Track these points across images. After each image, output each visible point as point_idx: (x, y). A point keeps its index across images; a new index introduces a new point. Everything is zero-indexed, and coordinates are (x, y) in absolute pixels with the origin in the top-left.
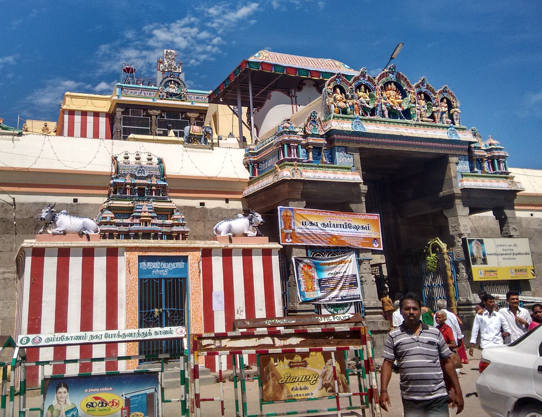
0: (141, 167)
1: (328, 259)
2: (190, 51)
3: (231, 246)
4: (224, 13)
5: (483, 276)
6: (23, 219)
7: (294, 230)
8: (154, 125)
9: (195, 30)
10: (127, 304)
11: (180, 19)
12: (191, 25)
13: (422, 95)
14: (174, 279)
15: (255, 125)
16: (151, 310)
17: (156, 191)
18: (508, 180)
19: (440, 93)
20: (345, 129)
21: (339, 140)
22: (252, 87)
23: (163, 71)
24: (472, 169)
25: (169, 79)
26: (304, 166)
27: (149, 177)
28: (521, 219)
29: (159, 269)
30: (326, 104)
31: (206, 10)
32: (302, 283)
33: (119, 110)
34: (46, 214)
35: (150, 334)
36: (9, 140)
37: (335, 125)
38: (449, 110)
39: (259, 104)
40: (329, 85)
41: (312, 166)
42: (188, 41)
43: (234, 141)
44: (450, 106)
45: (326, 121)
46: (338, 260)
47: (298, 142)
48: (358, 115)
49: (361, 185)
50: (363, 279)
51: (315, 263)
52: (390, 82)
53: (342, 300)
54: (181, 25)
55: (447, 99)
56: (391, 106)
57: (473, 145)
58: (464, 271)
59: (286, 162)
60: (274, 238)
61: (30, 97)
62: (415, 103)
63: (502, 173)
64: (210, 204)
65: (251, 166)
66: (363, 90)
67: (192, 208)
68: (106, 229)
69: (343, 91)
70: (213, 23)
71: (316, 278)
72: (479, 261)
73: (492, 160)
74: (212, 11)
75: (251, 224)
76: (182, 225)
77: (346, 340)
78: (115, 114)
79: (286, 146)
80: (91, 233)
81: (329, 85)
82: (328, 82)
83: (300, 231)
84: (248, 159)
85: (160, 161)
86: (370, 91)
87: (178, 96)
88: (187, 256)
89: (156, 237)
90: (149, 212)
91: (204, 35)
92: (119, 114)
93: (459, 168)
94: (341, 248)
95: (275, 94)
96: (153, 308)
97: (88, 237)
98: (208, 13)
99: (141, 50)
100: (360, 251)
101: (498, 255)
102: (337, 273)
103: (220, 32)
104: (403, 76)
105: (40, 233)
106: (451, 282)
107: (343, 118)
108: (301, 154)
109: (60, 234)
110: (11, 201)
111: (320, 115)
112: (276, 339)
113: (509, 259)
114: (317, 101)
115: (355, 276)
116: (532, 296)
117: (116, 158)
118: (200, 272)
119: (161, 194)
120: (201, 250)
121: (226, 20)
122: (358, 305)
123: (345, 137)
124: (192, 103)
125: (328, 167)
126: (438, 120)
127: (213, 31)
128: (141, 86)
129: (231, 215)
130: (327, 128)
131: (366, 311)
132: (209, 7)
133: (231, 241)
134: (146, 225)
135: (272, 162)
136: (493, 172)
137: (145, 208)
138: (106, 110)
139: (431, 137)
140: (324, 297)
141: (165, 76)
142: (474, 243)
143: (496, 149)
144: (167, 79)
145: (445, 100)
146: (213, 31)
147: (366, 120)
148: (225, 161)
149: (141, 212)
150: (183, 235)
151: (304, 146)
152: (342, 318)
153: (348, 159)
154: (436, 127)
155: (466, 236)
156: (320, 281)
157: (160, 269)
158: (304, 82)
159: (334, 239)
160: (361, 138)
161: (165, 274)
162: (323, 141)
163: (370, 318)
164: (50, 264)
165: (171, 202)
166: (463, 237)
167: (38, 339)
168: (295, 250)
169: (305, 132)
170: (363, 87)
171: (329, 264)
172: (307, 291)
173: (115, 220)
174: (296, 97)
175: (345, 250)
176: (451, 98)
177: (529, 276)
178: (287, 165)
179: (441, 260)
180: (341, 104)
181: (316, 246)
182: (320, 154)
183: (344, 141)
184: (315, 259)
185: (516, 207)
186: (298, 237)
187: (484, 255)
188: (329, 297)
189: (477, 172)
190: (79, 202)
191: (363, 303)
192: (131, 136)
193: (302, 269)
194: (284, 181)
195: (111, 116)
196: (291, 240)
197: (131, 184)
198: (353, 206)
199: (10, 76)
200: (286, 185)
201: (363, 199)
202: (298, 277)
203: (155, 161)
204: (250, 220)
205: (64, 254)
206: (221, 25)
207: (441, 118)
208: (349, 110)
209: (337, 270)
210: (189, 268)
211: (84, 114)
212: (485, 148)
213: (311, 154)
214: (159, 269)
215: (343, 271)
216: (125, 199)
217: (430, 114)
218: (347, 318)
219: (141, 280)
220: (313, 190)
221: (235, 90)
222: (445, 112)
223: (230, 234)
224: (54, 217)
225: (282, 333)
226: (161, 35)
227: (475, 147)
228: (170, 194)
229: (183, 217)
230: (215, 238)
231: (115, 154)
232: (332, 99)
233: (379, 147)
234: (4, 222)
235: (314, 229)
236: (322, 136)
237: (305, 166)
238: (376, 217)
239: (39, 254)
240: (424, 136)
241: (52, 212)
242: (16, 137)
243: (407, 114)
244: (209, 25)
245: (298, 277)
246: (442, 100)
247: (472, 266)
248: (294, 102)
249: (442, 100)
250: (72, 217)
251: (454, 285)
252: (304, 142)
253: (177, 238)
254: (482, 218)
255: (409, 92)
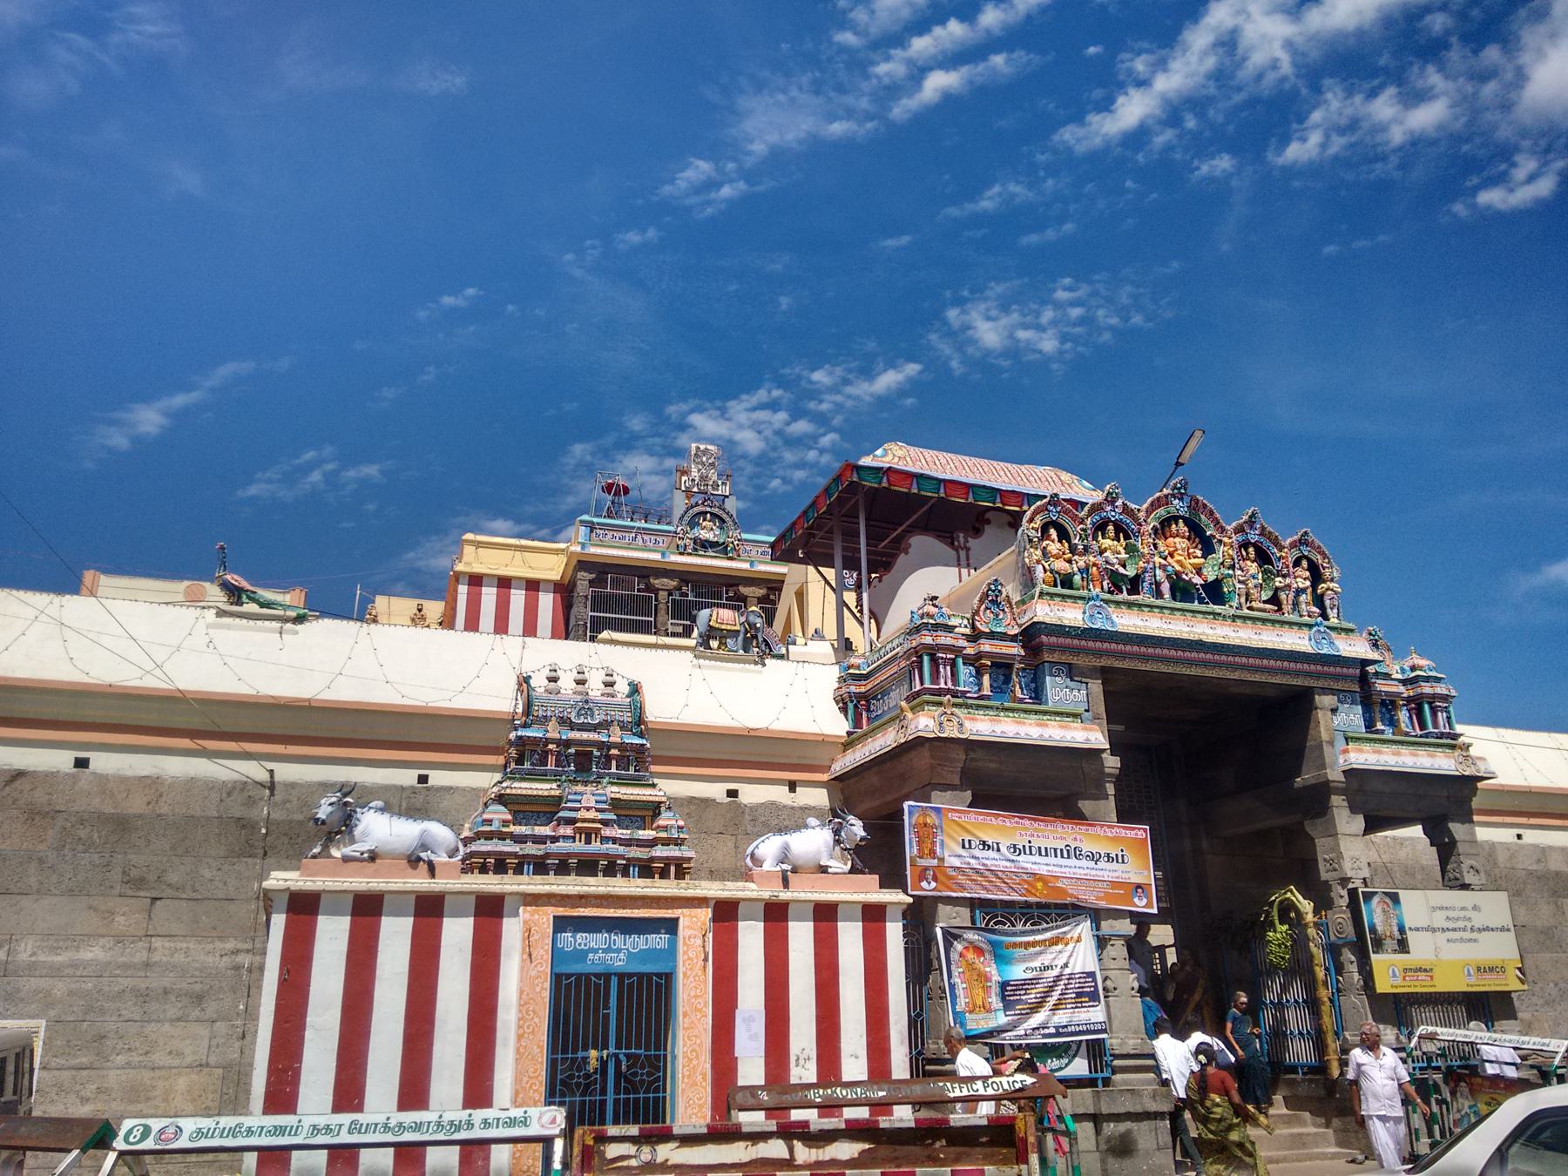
0: (587, 702)
1: (1023, 933)
2: (772, 462)
3: (785, 895)
4: (846, 382)
5: (1399, 981)
6: (291, 821)
7: (942, 860)
8: (662, 613)
9: (782, 416)
10: (520, 1037)
11: (748, 392)
12: (773, 406)
13: (1251, 550)
14: (640, 976)
15: (871, 611)
16: (580, 1054)
17: (618, 758)
18: (1457, 753)
19: (1293, 545)
20: (1067, 623)
21: (1053, 648)
22: (868, 524)
23: (688, 491)
24: (1370, 726)
25: (701, 508)
26: (968, 706)
27: (605, 725)
28: (1493, 846)
29: (604, 951)
30: (1024, 564)
31: (805, 373)
32: (960, 992)
33: (584, 577)
34: (330, 809)
35: (470, 1125)
36: (272, 631)
37: (1043, 612)
38: (1314, 586)
39: (883, 563)
40: (1031, 520)
41: (987, 707)
42: (766, 439)
43: (824, 649)
44: (1316, 575)
45: (1023, 602)
46: (1048, 935)
47: (958, 651)
48: (1098, 590)
49: (1104, 755)
50: (1108, 983)
51: (990, 942)
52: (1175, 519)
53: (1058, 1034)
54: (748, 405)
55: (1310, 561)
56: (1177, 574)
57: (1371, 669)
58: (1354, 968)
59: (927, 697)
60: (893, 878)
61: (411, 555)
62: (1232, 567)
63: (1442, 736)
64: (751, 794)
65: (851, 706)
66: (1112, 534)
67: (706, 802)
68: (489, 848)
69: (1063, 535)
70: (821, 401)
71: (996, 978)
72: (1390, 944)
73: (1417, 705)
74: (819, 376)
75: (838, 842)
76: (678, 842)
77: (978, 1149)
78: (575, 585)
79: (926, 659)
80: (441, 858)
81: (1031, 520)
82: (1028, 514)
83: (956, 862)
84: (844, 690)
85: (635, 689)
86: (1127, 537)
87: (721, 548)
88: (677, 919)
89: (610, 871)
90: (598, 810)
91: (802, 427)
92: (583, 587)
93: (1339, 720)
94: (1057, 906)
95: (920, 543)
96: (585, 1049)
97: (432, 869)
98: (811, 382)
99: (661, 456)
100: (1103, 915)
101: (1434, 930)
102: (1046, 968)
103: (837, 421)
104: (1205, 506)
105: (314, 857)
106: (1324, 994)
107: (1063, 597)
108: (962, 678)
109: (363, 860)
110: (263, 776)
111: (1011, 590)
112: (798, 1145)
113: (1462, 940)
114: (1007, 556)
115: (1092, 975)
116: (1521, 1033)
117: (527, 680)
118: (706, 959)
119: (632, 769)
120: (712, 903)
121: (849, 397)
122: (1096, 1051)
123: (1068, 641)
124: (752, 564)
125: (1025, 711)
126: (1287, 607)
127: (821, 420)
128: (643, 524)
129: (792, 821)
130: (1025, 620)
131: (1116, 1063)
132: (813, 370)
133: (786, 883)
134: (588, 842)
135: (897, 698)
136: (1419, 732)
137: (589, 799)
138: (556, 575)
139: (1270, 646)
140: (1012, 1026)
141: (693, 501)
142: (1376, 900)
143: (1427, 679)
144: (696, 510)
145: (1305, 563)
146: (821, 420)
147: (1118, 603)
148: (793, 694)
149: (578, 810)
150: (678, 867)
151: (974, 661)
152: (1006, 1087)
153: (1075, 692)
154: (1283, 623)
155: (1358, 883)
156: (1004, 985)
157: (608, 950)
158: (988, 515)
159: (1039, 885)
160: (1106, 645)
161: (619, 962)
162: (1016, 650)
163: (1125, 1082)
164: (332, 934)
165: (654, 786)
166: (1351, 886)
167: (172, 1130)
168: (943, 910)
169: (973, 627)
170: (1111, 527)
171: (1027, 945)
172: (971, 1012)
173: (512, 828)
174: (968, 549)
175: (1068, 911)
176: (1319, 559)
177: (1511, 983)
178: (928, 703)
179: (1299, 942)
180: (1060, 565)
181: (994, 901)
182: (1008, 679)
183: (1064, 649)
184: (993, 931)
185: (1475, 818)
186: (951, 878)
187: (1402, 930)
188: (1025, 1026)
189: (1382, 732)
190: (431, 782)
191: (1108, 1043)
192: (605, 635)
193: (961, 955)
194: (919, 742)
195: (564, 590)
196: (933, 884)
197: (559, 742)
198: (1086, 806)
199: (371, 507)
200: (925, 752)
201: (1110, 789)
202: (950, 977)
203: (622, 688)
204: (837, 832)
205: (367, 908)
206: (839, 407)
207: (1296, 604)
208: (1077, 578)
209: (1046, 959)
210: (681, 948)
211: (504, 583)
212: (1399, 676)
213: (986, 679)
214: (604, 951)
215: (1061, 962)
216: (542, 777)
217: (1270, 593)
218: (1018, 1086)
219: (557, 979)
220: (990, 764)
221: (830, 532)
222: (1304, 590)
223: (785, 867)
224: (350, 817)
225: (813, 1128)
226: (705, 423)
227: (1377, 673)
228: (653, 768)
229: (681, 823)
230: (747, 876)
231: (526, 669)
232: (1039, 552)
233: (1149, 667)
234: (244, 827)
235: (991, 859)
236: (1013, 638)
237: (971, 706)
238: (1141, 832)
239: (304, 907)
240: (1254, 644)
241: (346, 804)
242: (289, 625)
243: (1214, 591)
244: (812, 405)
245: (950, 977)
246: (1297, 563)
247: (1373, 957)
248: (965, 560)
249: (1297, 563)
250: (395, 818)
251: (1331, 1001)
252: (970, 651)
253: (664, 874)
254: (1401, 842)
255: (1220, 541)
